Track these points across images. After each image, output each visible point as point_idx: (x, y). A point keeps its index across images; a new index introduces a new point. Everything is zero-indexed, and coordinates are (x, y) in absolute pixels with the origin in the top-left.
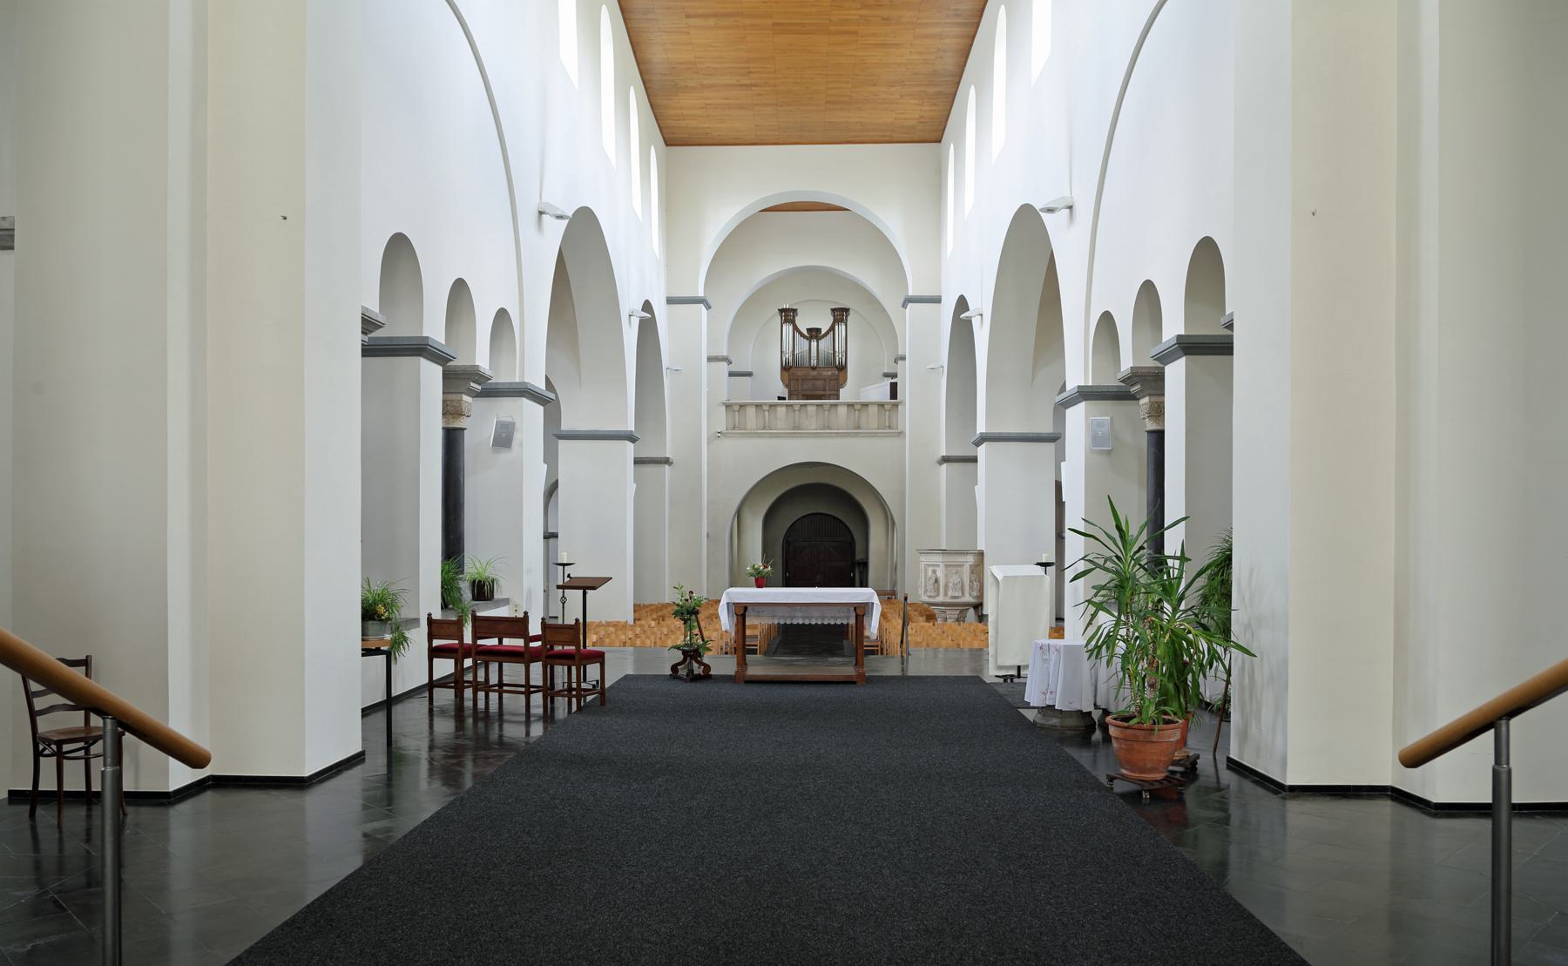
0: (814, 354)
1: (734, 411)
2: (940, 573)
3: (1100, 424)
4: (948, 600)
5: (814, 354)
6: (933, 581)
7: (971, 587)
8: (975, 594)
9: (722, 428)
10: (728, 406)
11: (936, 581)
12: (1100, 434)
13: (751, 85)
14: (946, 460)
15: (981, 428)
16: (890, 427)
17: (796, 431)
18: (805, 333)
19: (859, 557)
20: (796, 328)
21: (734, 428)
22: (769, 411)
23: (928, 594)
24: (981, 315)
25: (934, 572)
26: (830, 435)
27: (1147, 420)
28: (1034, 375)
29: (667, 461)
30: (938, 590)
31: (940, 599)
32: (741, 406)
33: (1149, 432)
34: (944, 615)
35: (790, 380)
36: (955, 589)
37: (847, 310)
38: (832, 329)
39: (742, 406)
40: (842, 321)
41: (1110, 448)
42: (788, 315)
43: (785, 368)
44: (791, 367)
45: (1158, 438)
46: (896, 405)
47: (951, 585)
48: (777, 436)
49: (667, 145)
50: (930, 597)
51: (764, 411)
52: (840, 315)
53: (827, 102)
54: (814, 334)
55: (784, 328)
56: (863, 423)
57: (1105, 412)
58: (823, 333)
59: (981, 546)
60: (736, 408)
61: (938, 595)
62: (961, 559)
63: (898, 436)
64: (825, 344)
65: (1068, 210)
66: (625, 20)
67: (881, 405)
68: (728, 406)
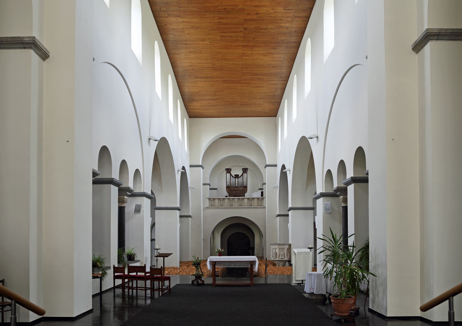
0: (237, 183)
2: (277, 251)
3: (327, 204)
5: (237, 183)
6: (275, 253)
7: (287, 255)
8: (288, 257)
9: (207, 206)
10: (209, 199)
11: (276, 253)
14: (279, 215)
15: (290, 206)
16: (261, 205)
17: (231, 206)
18: (234, 176)
19: (251, 246)
20: (231, 175)
21: (211, 206)
23: (274, 257)
24: (290, 170)
25: (275, 251)
26: (242, 208)
27: (342, 203)
29: (190, 216)
30: (277, 256)
31: (277, 259)
32: (213, 199)
33: (343, 207)
34: (279, 264)
35: (229, 191)
36: (282, 256)
37: (247, 169)
38: (242, 175)
39: (214, 199)
40: (245, 172)
41: (330, 212)
42: (228, 171)
43: (228, 187)
44: (230, 187)
46: (263, 199)
47: (281, 255)
48: (225, 208)
49: (190, 117)
50: (274, 258)
51: (221, 200)
52: (245, 170)
54: (237, 176)
55: (227, 174)
56: (252, 204)
57: (329, 201)
58: (240, 176)
59: (290, 242)
60: (212, 200)
61: (277, 258)
62: (284, 246)
64: (240, 179)
65: (316, 138)
67: (258, 199)
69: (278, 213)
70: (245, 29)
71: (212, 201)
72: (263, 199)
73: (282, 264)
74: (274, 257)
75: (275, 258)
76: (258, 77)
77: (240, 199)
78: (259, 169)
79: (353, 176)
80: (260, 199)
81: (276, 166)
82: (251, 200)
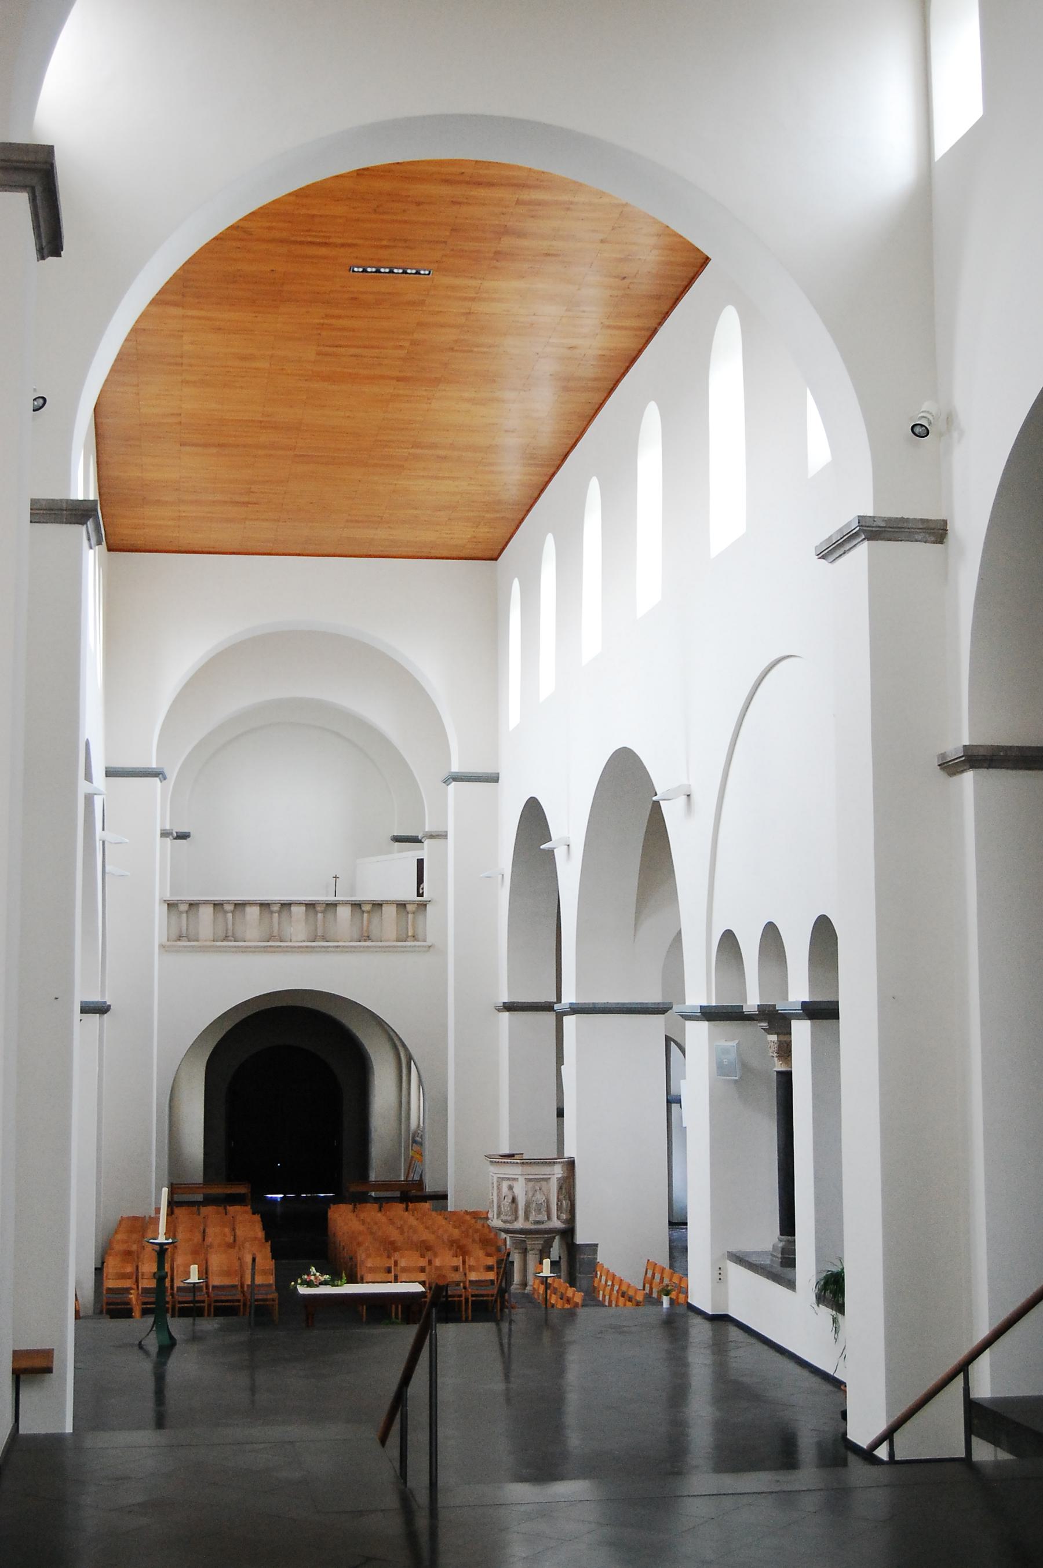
1: (181, 913)
2: (520, 1190)
3: (726, 1051)
4: (529, 1226)
8: (564, 1216)
10: (171, 905)
11: (514, 1200)
12: (725, 1061)
13: (248, 503)
14: (510, 1007)
15: (569, 997)
22: (233, 912)
23: (503, 1217)
24: (568, 845)
25: (511, 1188)
27: (776, 1059)
28: (637, 919)
30: (516, 1211)
31: (519, 1224)
32: (191, 905)
33: (778, 1073)
39: (193, 905)
41: (737, 1078)
45: (785, 1080)
46: (423, 906)
48: (245, 950)
50: (505, 1222)
51: (226, 912)
53: (347, 521)
57: (730, 1036)
59: (570, 1151)
60: (184, 907)
61: (516, 1219)
62: (546, 1170)
63: (428, 951)
66: (97, 444)
67: (402, 905)
68: (171, 905)
69: (505, 998)
70: (414, 343)
71: (184, 915)
72: (426, 905)
73: (539, 1244)
74: (503, 1217)
75: (509, 1218)
76: (441, 453)
77: (318, 908)
78: (406, 765)
79: (807, 999)
80: (410, 908)
81: (494, 779)
82: (368, 912)
